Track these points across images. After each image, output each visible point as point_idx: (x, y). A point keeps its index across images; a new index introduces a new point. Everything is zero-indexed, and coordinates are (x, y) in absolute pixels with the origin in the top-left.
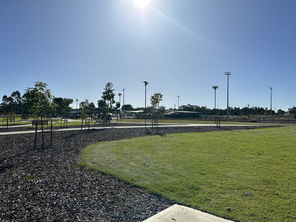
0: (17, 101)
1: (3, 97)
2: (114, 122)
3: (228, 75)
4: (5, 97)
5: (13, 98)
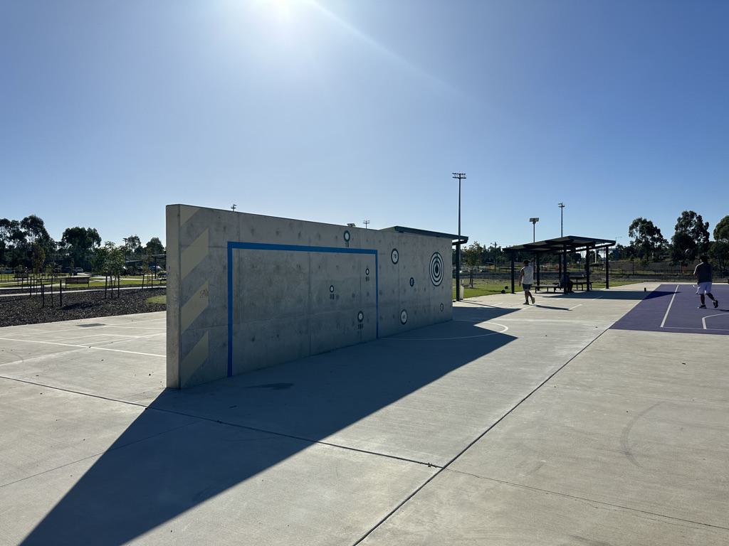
3: (460, 178)
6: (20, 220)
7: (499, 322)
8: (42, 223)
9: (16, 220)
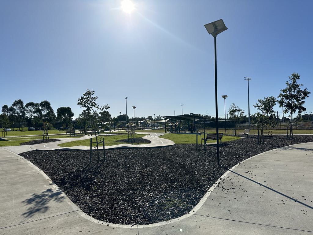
0: (19, 112)
1: (3, 107)
2: (121, 131)
3: (248, 80)
4: (5, 107)
5: (14, 108)
6: (39, 102)
7: (253, 161)
8: (49, 104)
9: (37, 103)
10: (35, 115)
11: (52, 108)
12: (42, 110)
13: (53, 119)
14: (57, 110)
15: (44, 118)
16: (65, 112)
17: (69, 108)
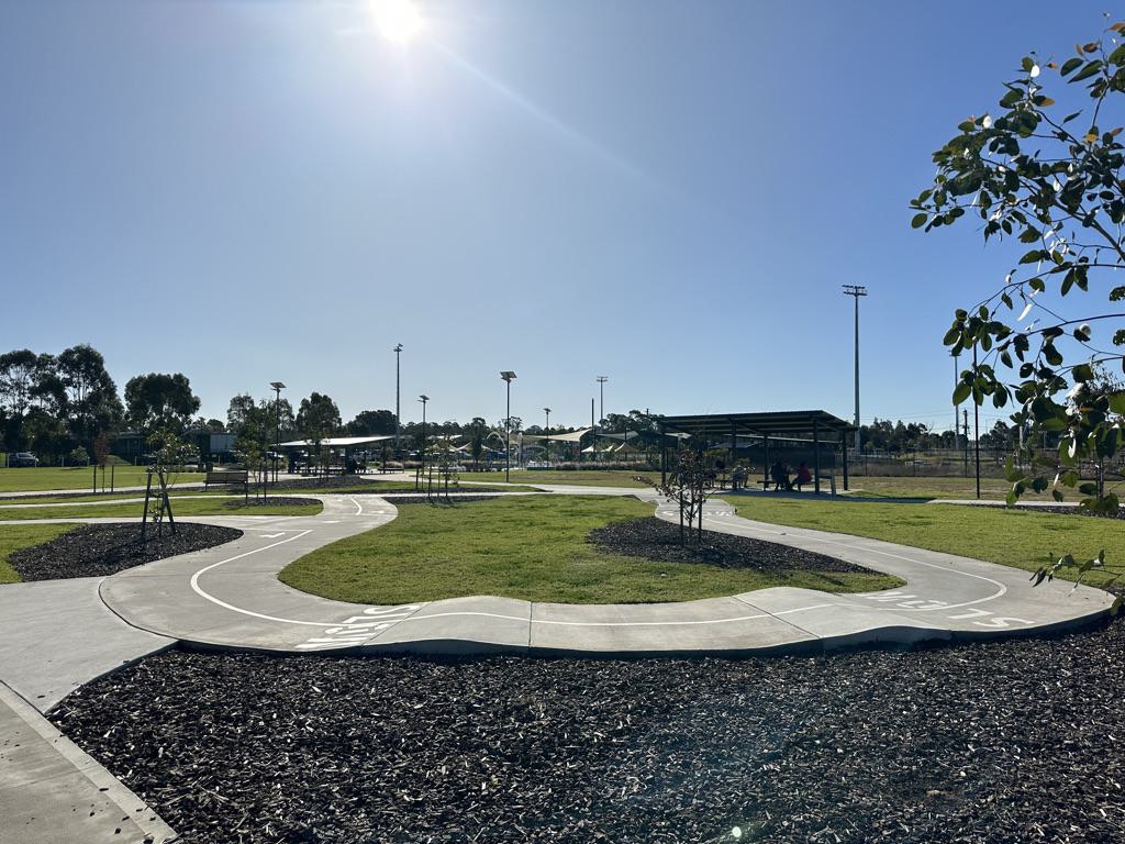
6: (57, 353)
9: (49, 354)
10: (37, 402)
11: (110, 376)
12: (69, 383)
13: (111, 419)
14: (128, 386)
15: (75, 416)
16: (163, 394)
17: (179, 378)
